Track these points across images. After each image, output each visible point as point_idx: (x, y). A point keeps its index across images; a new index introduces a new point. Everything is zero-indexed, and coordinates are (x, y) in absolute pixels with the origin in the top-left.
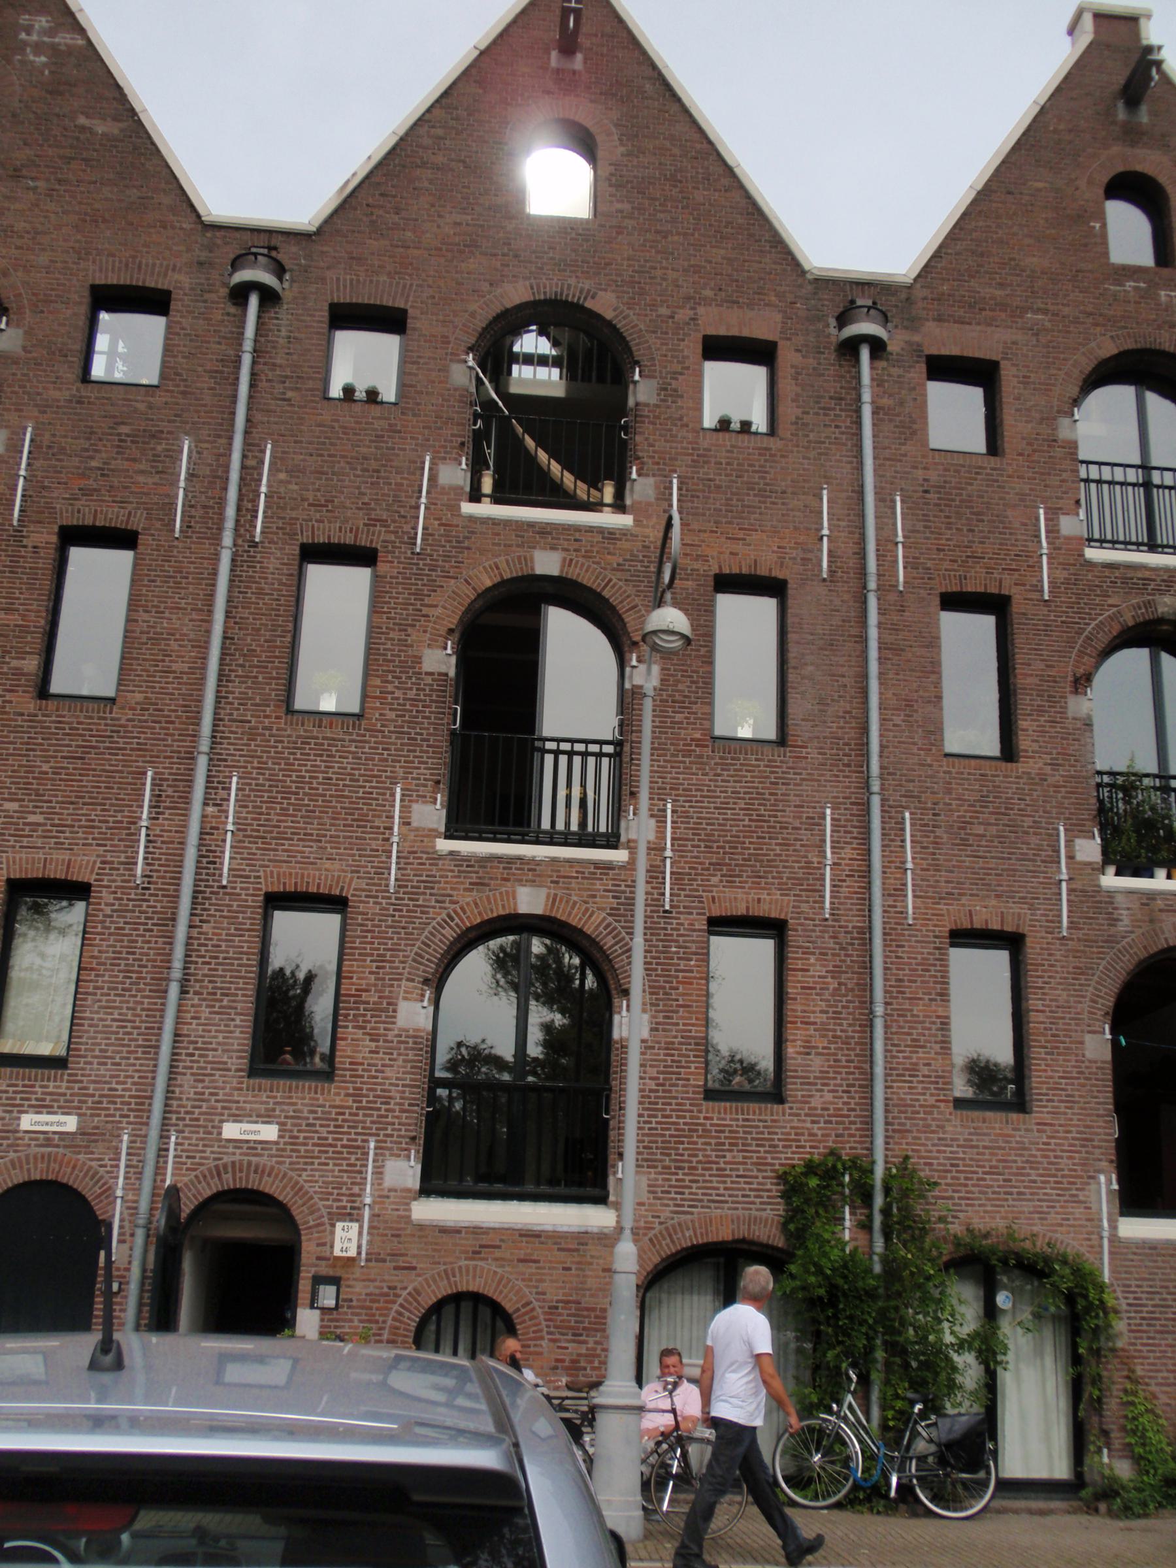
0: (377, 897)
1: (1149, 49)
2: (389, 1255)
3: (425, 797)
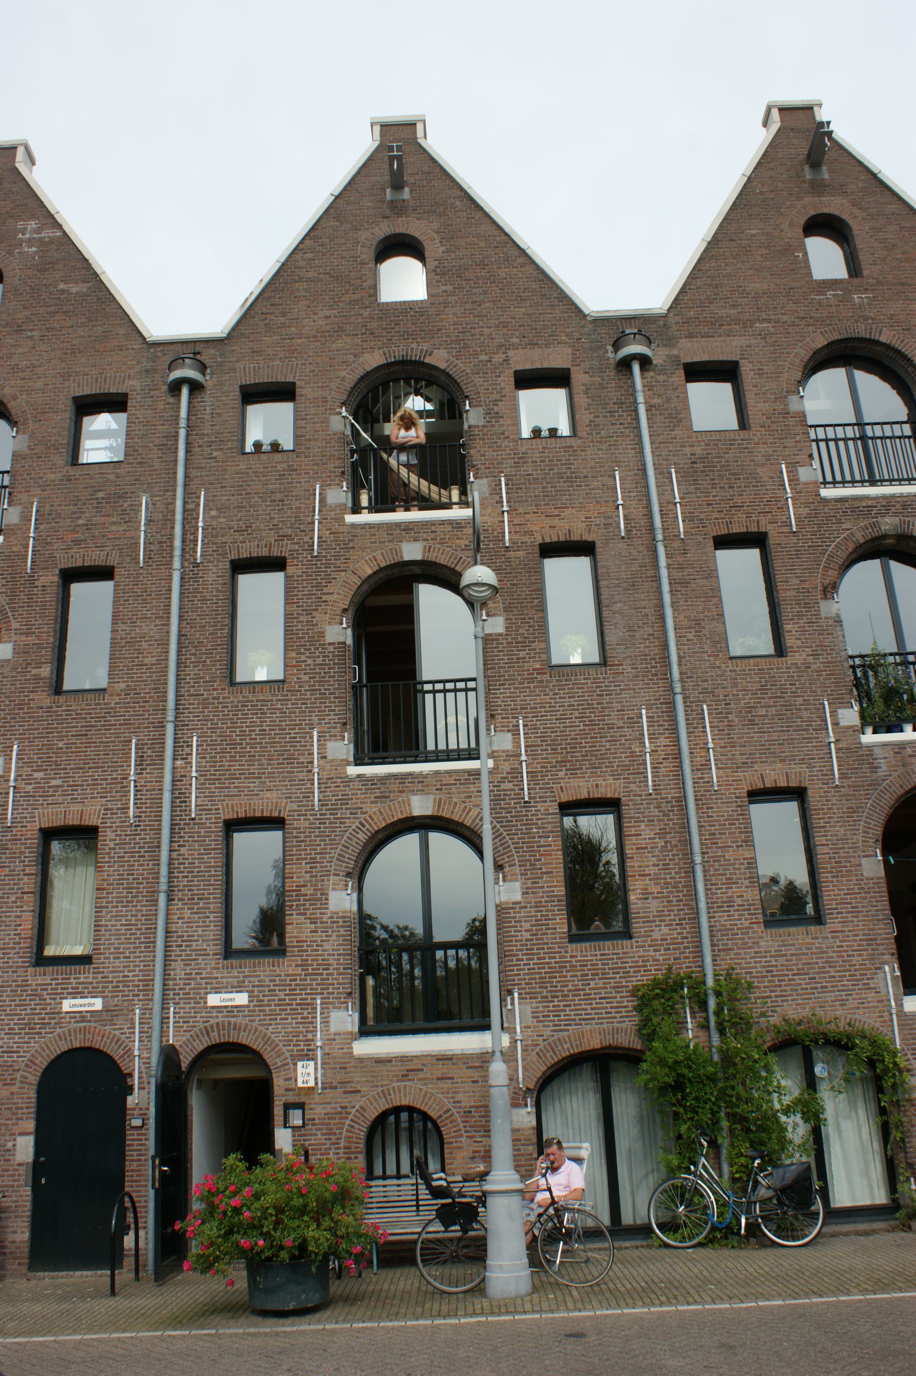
0: (306, 815)
1: (821, 124)
2: (339, 1083)
3: (336, 736)
